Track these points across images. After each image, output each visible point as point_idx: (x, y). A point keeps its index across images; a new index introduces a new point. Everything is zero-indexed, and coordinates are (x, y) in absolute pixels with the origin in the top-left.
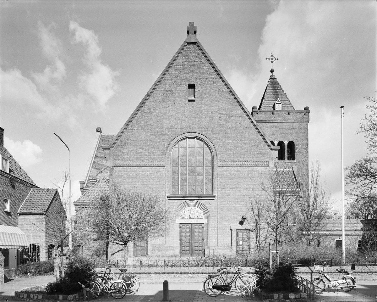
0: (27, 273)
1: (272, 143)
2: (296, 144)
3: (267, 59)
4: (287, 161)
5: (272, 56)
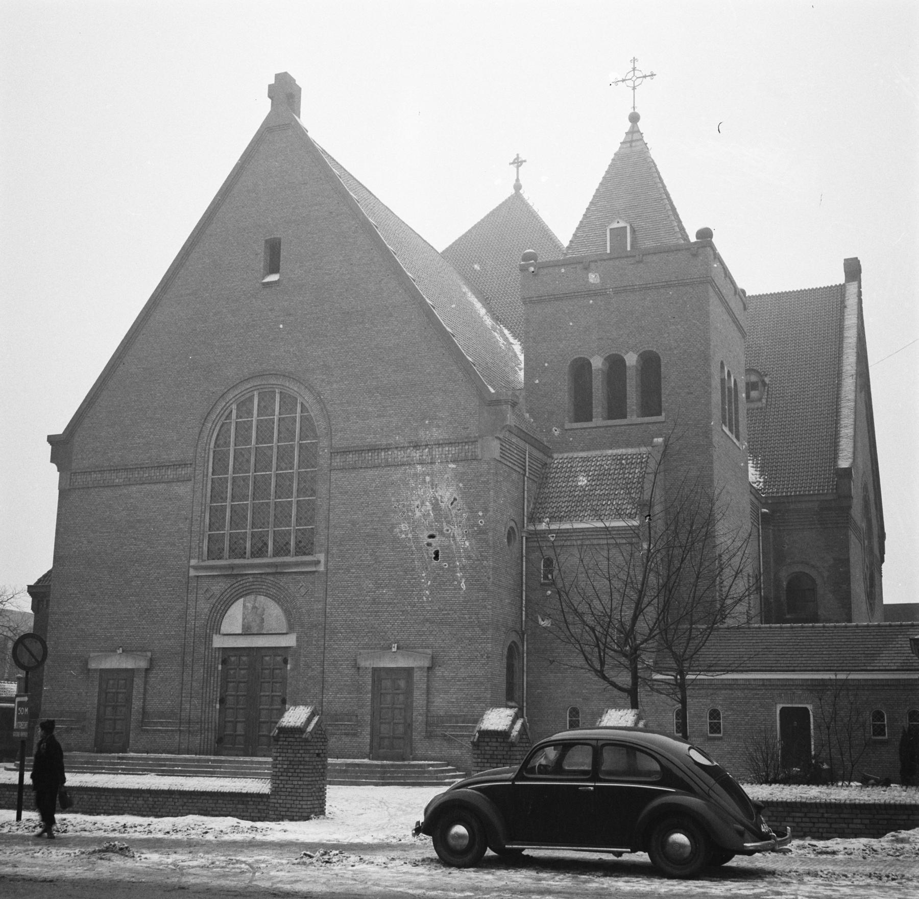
2: (664, 361)
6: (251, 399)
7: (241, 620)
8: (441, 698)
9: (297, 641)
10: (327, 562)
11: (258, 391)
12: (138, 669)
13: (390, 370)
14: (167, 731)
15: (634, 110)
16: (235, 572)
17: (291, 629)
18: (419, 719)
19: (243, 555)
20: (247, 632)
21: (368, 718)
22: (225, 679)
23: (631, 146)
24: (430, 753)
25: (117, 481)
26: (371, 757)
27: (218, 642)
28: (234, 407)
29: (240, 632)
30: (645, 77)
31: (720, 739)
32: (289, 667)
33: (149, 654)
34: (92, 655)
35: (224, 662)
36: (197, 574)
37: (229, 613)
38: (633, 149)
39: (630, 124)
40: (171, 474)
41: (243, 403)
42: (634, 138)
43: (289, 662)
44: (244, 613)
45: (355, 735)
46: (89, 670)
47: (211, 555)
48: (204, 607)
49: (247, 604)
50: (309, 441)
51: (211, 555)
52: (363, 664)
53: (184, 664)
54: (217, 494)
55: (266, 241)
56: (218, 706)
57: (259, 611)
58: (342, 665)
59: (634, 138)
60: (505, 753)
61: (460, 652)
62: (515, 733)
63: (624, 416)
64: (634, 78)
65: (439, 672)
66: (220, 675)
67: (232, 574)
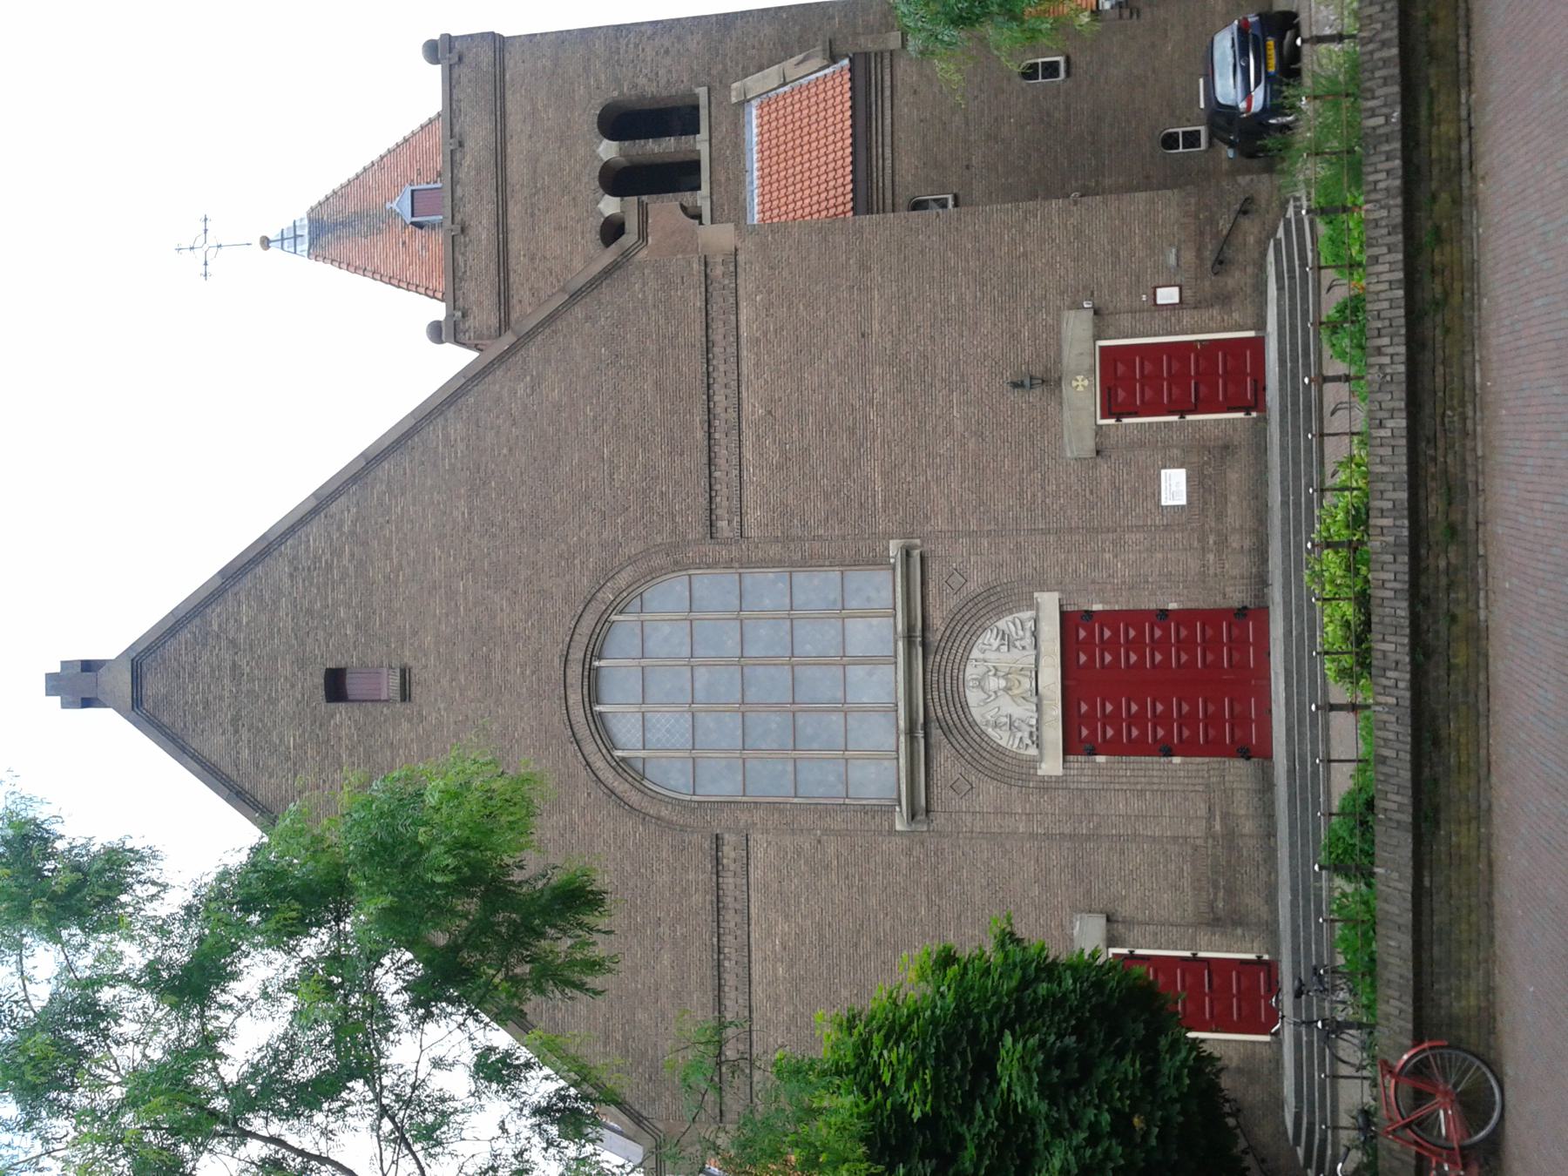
59: (289, 238)
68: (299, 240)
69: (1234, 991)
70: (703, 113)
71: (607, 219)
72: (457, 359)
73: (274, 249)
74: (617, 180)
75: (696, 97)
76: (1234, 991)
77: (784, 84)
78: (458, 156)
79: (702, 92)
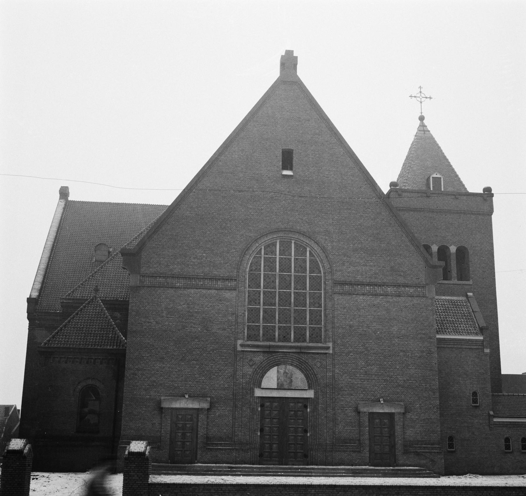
0: (492, 393)
1: (427, 248)
2: (471, 252)
3: (420, 87)
4: (456, 281)
5: (421, 92)
6: (274, 245)
7: (276, 379)
8: (411, 431)
9: (315, 395)
10: (334, 348)
11: (279, 240)
12: (202, 409)
13: (369, 240)
14: (226, 449)
15: (421, 113)
16: (271, 350)
17: (310, 388)
18: (399, 442)
19: (273, 340)
20: (280, 387)
21: (367, 442)
22: (263, 417)
23: (425, 133)
24: (407, 462)
25: (178, 284)
26: (370, 465)
27: (258, 393)
28: (263, 248)
29: (276, 387)
30: (415, 97)
31: (509, 453)
32: (308, 410)
33: (209, 399)
34: (162, 398)
35: (262, 406)
36: (242, 350)
37: (267, 375)
38: (426, 135)
39: (420, 121)
40: (220, 284)
41: (268, 246)
42: (423, 129)
43: (308, 407)
44: (277, 376)
45: (359, 452)
46: (162, 408)
47: (249, 338)
48: (249, 370)
49: (280, 371)
50: (315, 275)
51: (249, 338)
52: (364, 409)
53: (235, 406)
54: (253, 299)
55: (293, 150)
56: (259, 434)
57: (289, 375)
58: (346, 410)
59: (423, 129)
60: (144, 466)
61: (421, 404)
62: (25, 451)
63: (450, 279)
64: (421, 97)
65: (408, 416)
66: (259, 414)
67: (269, 351)
68: (423, 132)
69: (499, 394)
70: (464, 282)
71: (430, 247)
72: (385, 189)
73: (419, 122)
74: (443, 252)
75: (468, 280)
76: (499, 394)
77: (473, 311)
78: (453, 197)
79: (471, 282)
